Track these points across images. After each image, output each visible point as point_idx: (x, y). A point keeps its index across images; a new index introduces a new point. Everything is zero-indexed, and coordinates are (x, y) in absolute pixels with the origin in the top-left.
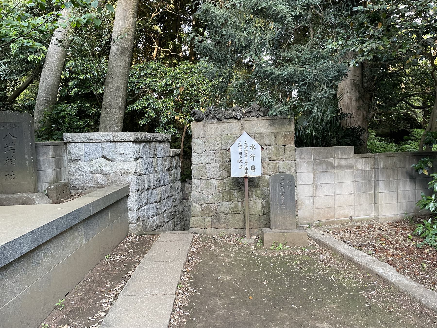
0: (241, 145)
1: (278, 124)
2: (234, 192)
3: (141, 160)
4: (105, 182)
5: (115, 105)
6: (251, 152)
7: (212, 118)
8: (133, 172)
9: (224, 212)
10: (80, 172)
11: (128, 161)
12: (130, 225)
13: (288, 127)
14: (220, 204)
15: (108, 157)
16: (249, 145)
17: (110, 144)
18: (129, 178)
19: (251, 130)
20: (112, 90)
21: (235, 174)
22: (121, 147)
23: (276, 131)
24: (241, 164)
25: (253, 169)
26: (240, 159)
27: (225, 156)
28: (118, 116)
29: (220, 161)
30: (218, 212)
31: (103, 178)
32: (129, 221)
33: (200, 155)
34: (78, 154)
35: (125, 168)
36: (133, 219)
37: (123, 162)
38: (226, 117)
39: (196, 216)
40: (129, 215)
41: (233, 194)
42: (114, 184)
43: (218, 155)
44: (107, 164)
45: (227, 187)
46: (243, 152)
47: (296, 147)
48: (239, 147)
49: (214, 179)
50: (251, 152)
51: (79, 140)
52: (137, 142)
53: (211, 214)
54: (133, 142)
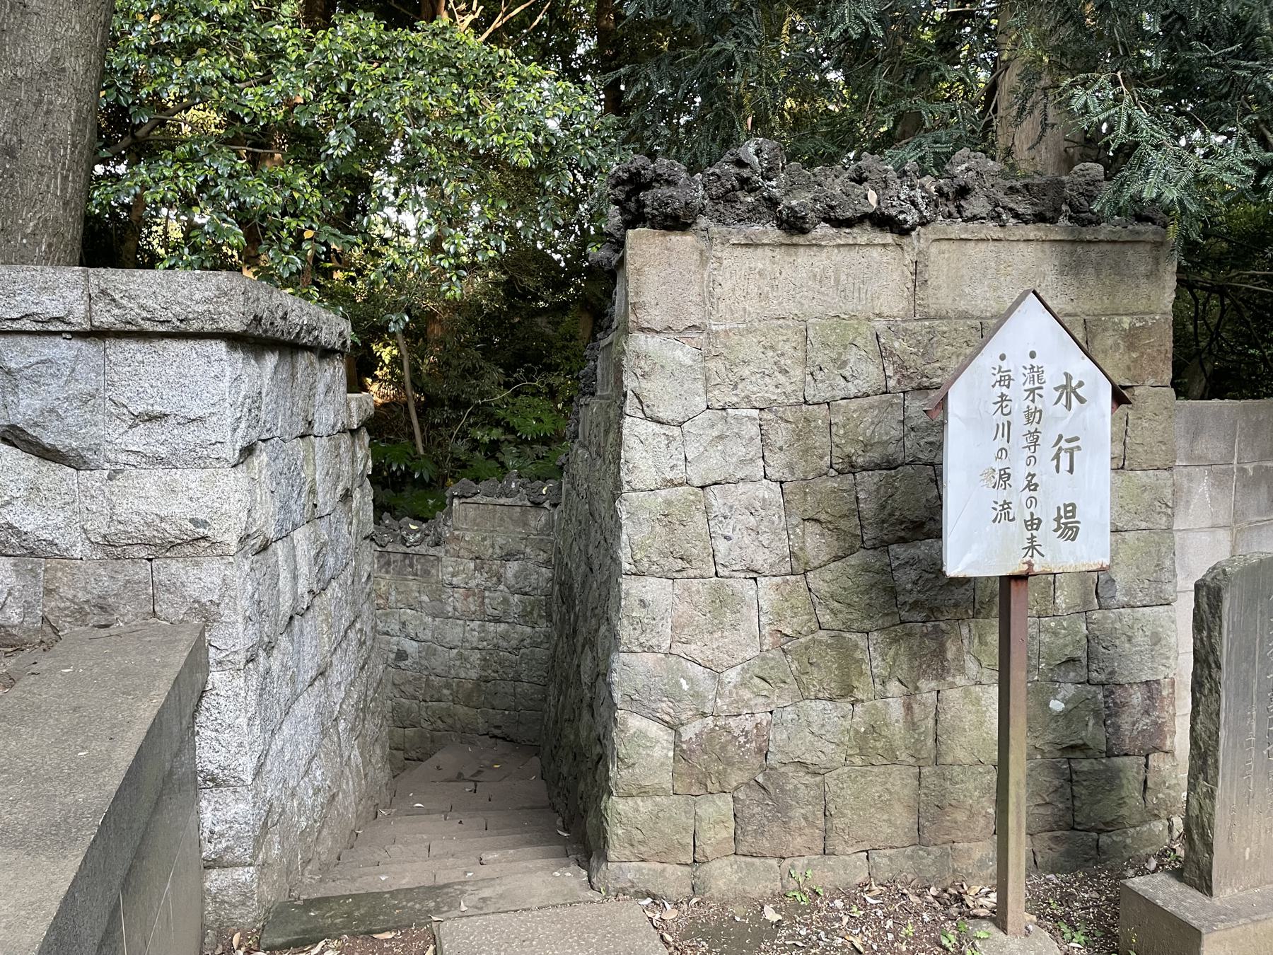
0: (1005, 380)
1: (1098, 272)
2: (863, 644)
3: (262, 458)
4: (28, 608)
5: (37, 153)
6: (1059, 420)
7: (752, 215)
8: (232, 539)
9: (808, 758)
11: (200, 462)
12: (215, 880)
13: (1145, 287)
14: (789, 714)
15: (48, 439)
16: (1053, 378)
17: (63, 349)
18: (202, 579)
19: (962, 295)
20: (20, 72)
21: (968, 558)
22: (148, 374)
23: (1087, 306)
24: (1001, 495)
25: (1068, 527)
26: (998, 465)
27: (820, 440)
28: (54, 210)
29: (791, 467)
30: (773, 760)
32: (209, 850)
33: (676, 431)
35: (177, 510)
36: (237, 838)
37: (159, 471)
38: (839, 214)
39: (644, 792)
40: (208, 817)
41: (858, 655)
42: (94, 620)
43: (781, 435)
44: (45, 482)
45: (826, 618)
46: (1018, 420)
47: (1179, 394)
48: (998, 390)
49: (754, 574)
52: (251, 341)
53: (735, 778)
54: (234, 340)
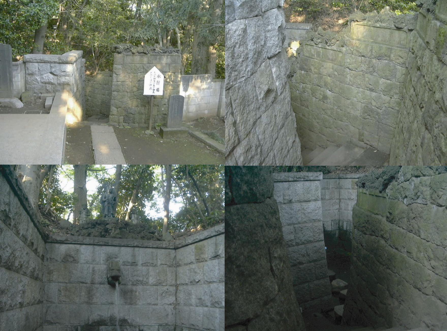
10: (34, 82)
25: (158, 90)
31: (50, 87)
34: (34, 70)
39: (113, 115)
50: (157, 79)
51: (35, 61)
